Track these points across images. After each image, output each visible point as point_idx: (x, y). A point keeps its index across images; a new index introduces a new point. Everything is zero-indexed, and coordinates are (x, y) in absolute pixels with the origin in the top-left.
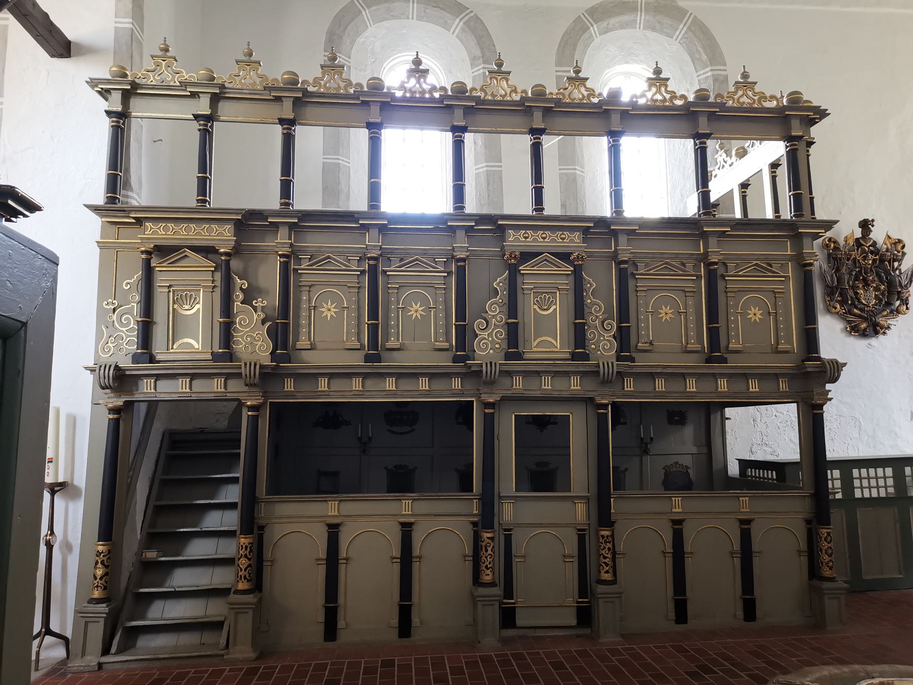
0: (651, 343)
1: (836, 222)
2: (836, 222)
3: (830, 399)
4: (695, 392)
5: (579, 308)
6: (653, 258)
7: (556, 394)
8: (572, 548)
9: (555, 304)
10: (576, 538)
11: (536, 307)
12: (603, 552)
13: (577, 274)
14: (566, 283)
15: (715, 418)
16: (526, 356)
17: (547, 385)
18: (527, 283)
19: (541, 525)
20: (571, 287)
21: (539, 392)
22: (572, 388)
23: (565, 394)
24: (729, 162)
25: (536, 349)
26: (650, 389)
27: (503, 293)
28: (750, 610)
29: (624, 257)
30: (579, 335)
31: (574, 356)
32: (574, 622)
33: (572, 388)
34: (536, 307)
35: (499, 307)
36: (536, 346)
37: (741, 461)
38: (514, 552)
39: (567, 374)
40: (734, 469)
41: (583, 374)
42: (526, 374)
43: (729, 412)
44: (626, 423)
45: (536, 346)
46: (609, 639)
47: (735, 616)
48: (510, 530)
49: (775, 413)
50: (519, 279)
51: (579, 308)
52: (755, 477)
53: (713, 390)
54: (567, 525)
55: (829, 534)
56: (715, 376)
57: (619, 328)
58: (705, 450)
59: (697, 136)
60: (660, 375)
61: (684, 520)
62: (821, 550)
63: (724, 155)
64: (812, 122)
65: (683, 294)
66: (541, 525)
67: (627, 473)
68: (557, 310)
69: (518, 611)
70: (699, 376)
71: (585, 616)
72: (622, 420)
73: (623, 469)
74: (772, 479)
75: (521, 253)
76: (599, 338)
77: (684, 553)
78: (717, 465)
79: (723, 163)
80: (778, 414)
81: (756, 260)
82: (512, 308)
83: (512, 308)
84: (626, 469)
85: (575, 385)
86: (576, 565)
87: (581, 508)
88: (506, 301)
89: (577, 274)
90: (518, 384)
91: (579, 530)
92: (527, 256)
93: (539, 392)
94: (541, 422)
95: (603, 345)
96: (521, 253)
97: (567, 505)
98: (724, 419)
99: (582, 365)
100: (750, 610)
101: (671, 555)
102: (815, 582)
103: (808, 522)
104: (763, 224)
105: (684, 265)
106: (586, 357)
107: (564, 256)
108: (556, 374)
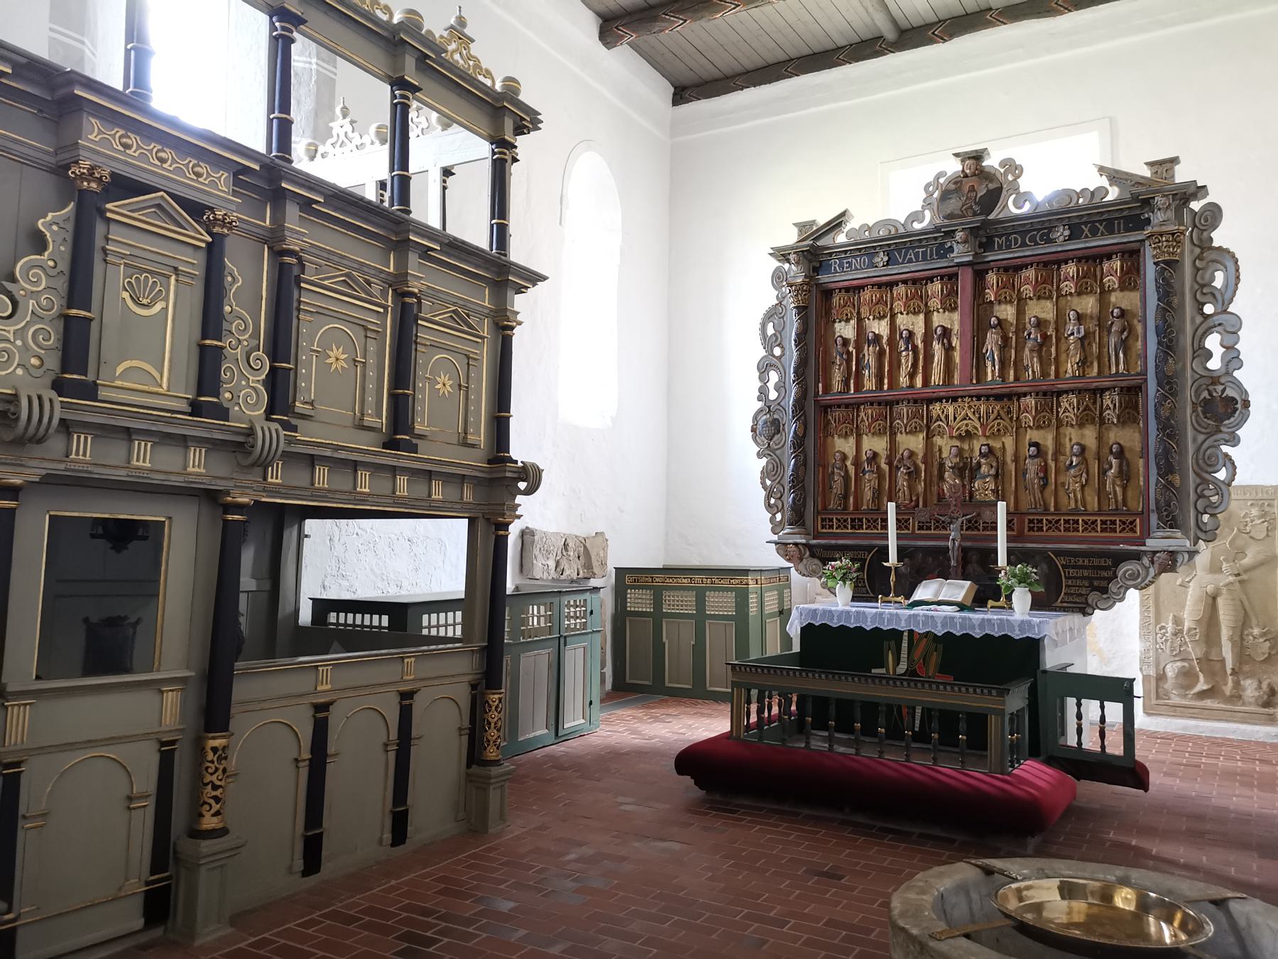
0: (312, 403)
1: (544, 278)
2: (544, 278)
3: (519, 517)
4: (329, 491)
5: (211, 319)
6: (328, 260)
7: (157, 478)
8: (147, 781)
9: (166, 299)
10: (155, 759)
11: (125, 295)
12: (214, 778)
13: (214, 252)
14: (194, 264)
15: (290, 535)
16: (103, 393)
17: (145, 459)
18: (119, 242)
19: (90, 744)
20: (199, 272)
21: (62, 466)
22: (190, 469)
23: (176, 481)
24: (357, 141)
25: (118, 383)
26: (305, 482)
27: (58, 249)
28: (399, 826)
29: (293, 244)
30: (208, 368)
31: (196, 409)
32: (139, 923)
33: (190, 469)
34: (125, 295)
35: (47, 275)
36: (122, 377)
37: (316, 602)
38: (22, 810)
39: (184, 441)
40: (305, 616)
41: (214, 445)
42: (103, 432)
43: (311, 525)
44: (145, 538)
45: (122, 377)
46: (210, 932)
47: (380, 842)
48: (17, 764)
49: (357, 530)
50: (100, 228)
51: (211, 319)
52: (346, 625)
53: (349, 487)
54: (145, 737)
55: (500, 700)
56: (394, 471)
57: (273, 370)
58: (267, 586)
59: (398, 83)
60: (325, 460)
61: (331, 703)
62: (489, 723)
63: (348, 128)
64: (520, 130)
65: (362, 333)
66: (90, 744)
67: (139, 628)
68: (169, 312)
69: (20, 934)
70: (376, 468)
71: (158, 906)
72: (140, 533)
73: (133, 620)
74: (380, 627)
75: (113, 174)
76: (239, 381)
77: (326, 755)
78: (285, 609)
79: (342, 137)
80: (360, 532)
81: (454, 304)
82: (79, 284)
83: (79, 284)
84: (138, 622)
85: (196, 465)
86: (151, 811)
87: (171, 699)
88: (64, 266)
89: (214, 252)
90: (83, 451)
91: (163, 744)
92: (125, 187)
93: (123, 472)
94: (121, 534)
95: (245, 393)
96: (113, 174)
97: (148, 697)
98: (301, 536)
99: (210, 428)
100: (399, 826)
101: (307, 763)
102: (475, 769)
103: (474, 687)
104: (458, 248)
105: (369, 283)
106: (222, 412)
107: (196, 210)
108: (165, 439)
